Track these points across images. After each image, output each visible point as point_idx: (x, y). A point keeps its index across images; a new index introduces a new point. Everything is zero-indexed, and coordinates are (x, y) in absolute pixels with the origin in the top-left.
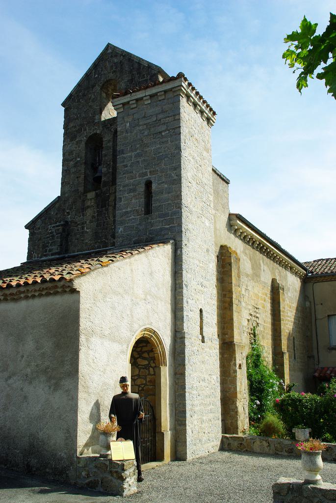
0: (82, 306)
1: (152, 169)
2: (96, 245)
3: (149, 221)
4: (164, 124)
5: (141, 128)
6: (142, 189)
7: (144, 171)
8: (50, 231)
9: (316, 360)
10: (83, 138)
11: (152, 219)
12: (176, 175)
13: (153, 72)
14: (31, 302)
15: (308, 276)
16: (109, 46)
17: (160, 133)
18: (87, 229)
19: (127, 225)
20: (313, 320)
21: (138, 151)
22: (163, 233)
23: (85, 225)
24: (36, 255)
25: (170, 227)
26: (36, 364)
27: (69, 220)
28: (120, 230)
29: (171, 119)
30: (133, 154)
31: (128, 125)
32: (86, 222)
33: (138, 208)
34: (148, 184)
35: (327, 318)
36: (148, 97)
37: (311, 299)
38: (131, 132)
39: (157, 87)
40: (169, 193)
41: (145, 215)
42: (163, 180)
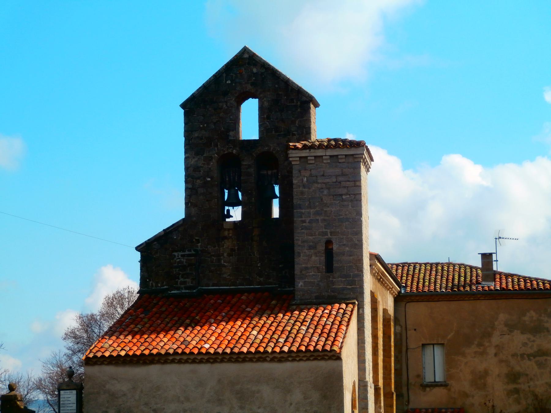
0: (344, 369)
1: (332, 230)
2: (238, 282)
3: (331, 279)
4: (345, 187)
5: (319, 186)
6: (321, 248)
7: (324, 230)
8: (178, 260)
9: (406, 398)
10: (214, 154)
11: (334, 278)
12: (357, 240)
13: (304, 99)
14: (295, 364)
15: (401, 294)
16: (245, 50)
17: (341, 195)
18: (224, 262)
19: (306, 280)
20: (404, 349)
21: (317, 209)
22: (345, 292)
23: (222, 257)
24: (154, 284)
25: (352, 288)
26: (304, 409)
27: (199, 248)
28: (300, 284)
29: (352, 184)
30: (312, 211)
31: (305, 179)
32: (223, 255)
33: (318, 266)
34: (329, 243)
35: (421, 347)
36: (328, 157)
37: (403, 323)
38: (309, 188)
39: (337, 149)
40: (350, 256)
41: (325, 273)
42: (344, 243)
